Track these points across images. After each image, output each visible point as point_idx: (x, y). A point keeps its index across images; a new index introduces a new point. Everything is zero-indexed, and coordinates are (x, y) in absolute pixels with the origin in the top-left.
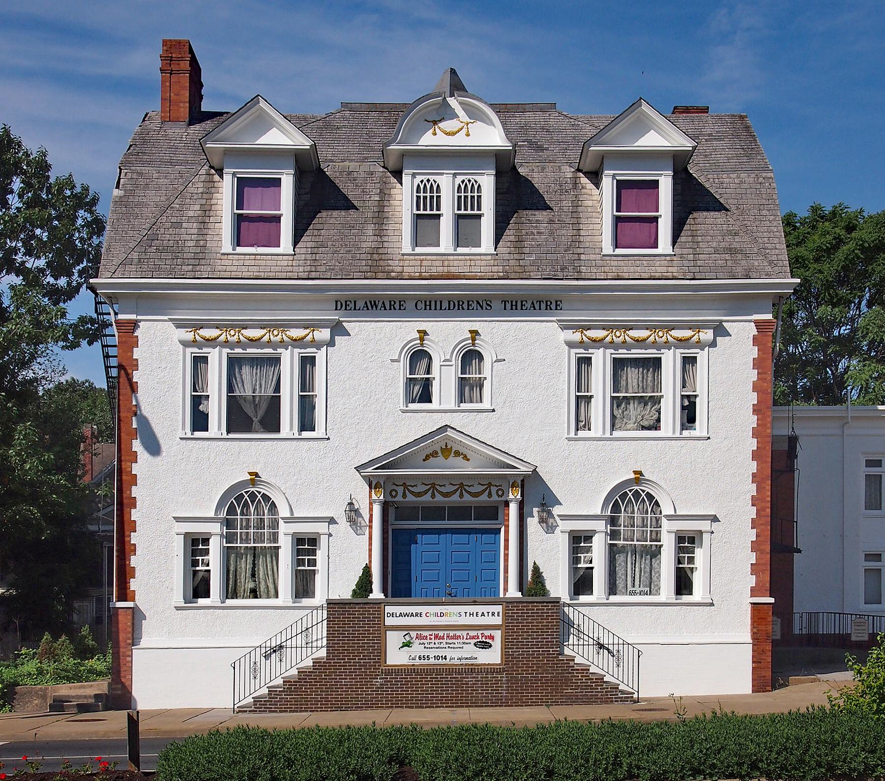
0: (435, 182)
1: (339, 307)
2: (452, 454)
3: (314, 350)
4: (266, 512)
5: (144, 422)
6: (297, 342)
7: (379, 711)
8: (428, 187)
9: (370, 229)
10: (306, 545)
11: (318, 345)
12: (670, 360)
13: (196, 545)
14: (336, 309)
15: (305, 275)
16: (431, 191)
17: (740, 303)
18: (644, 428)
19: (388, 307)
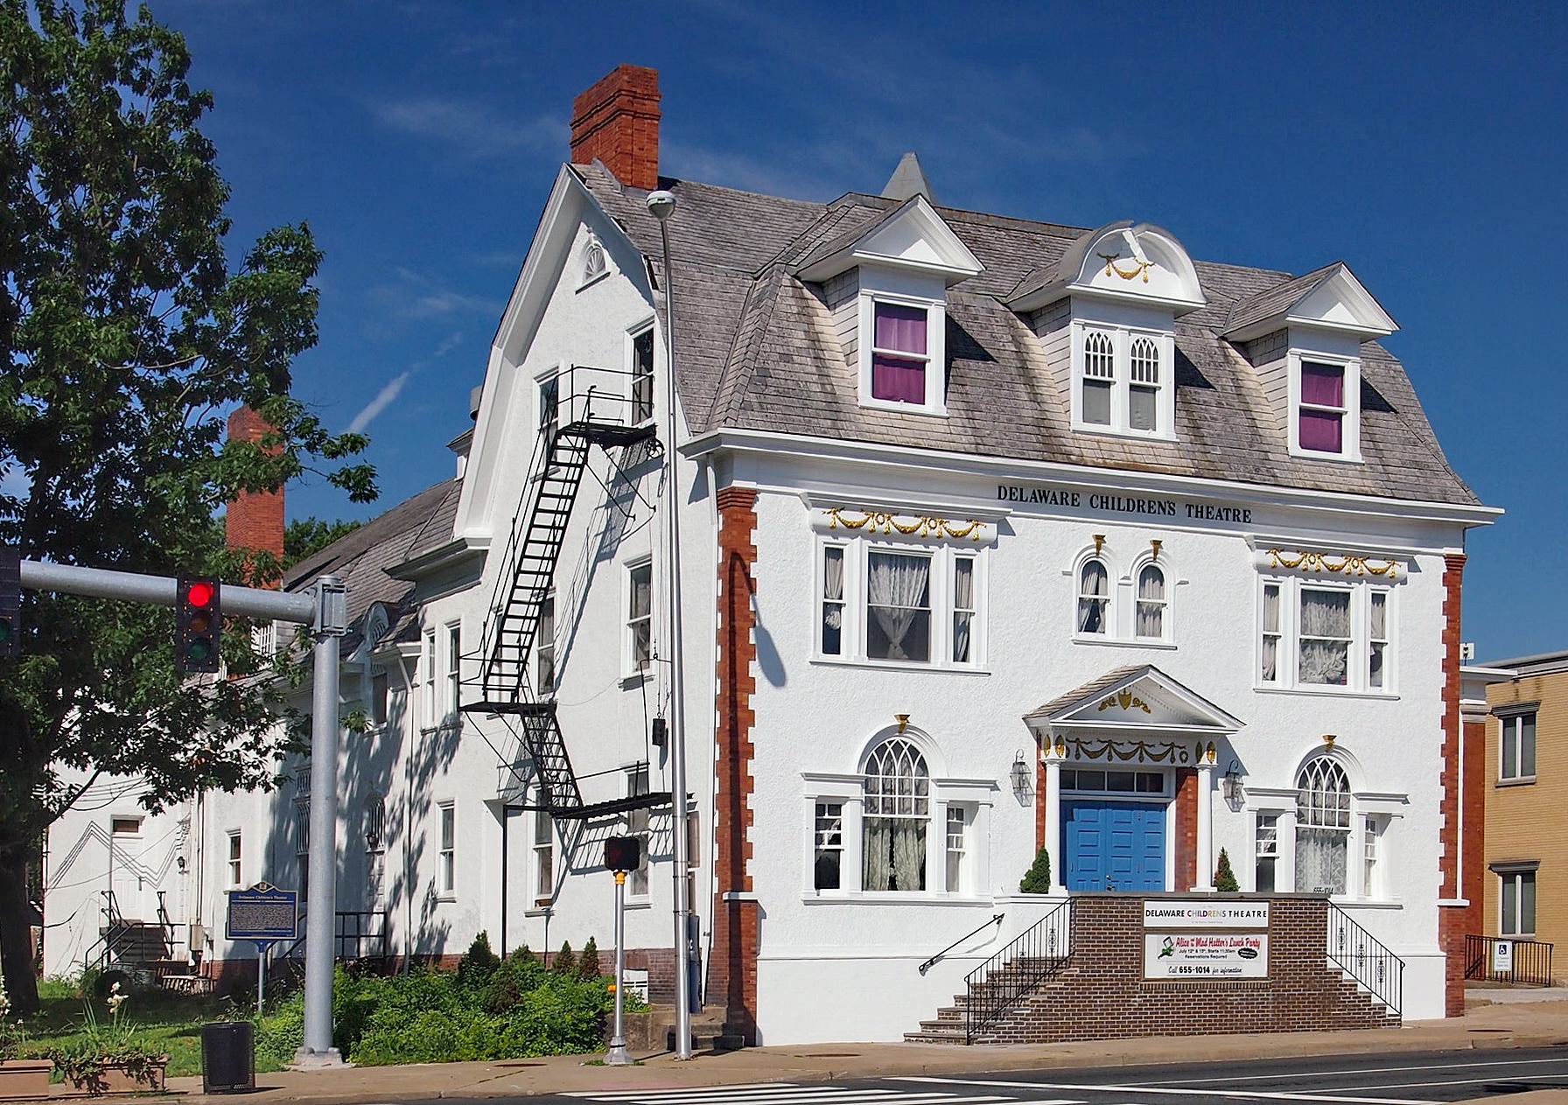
3: (973, 551)
5: (764, 636)
6: (958, 539)
7: (1138, 1039)
9: (1022, 392)
11: (978, 544)
12: (1360, 595)
13: (827, 811)
15: (972, 448)
17: (1432, 532)
18: (1330, 681)
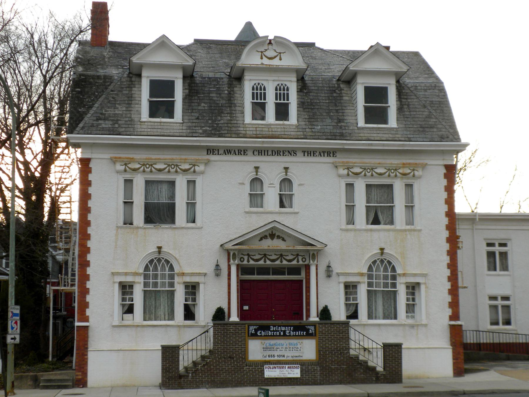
0: (263, 85)
1: (274, 154)
2: (276, 237)
4: (159, 269)
8: (282, 87)
10: (192, 289)
14: (207, 154)
16: (261, 90)
19: (237, 153)
